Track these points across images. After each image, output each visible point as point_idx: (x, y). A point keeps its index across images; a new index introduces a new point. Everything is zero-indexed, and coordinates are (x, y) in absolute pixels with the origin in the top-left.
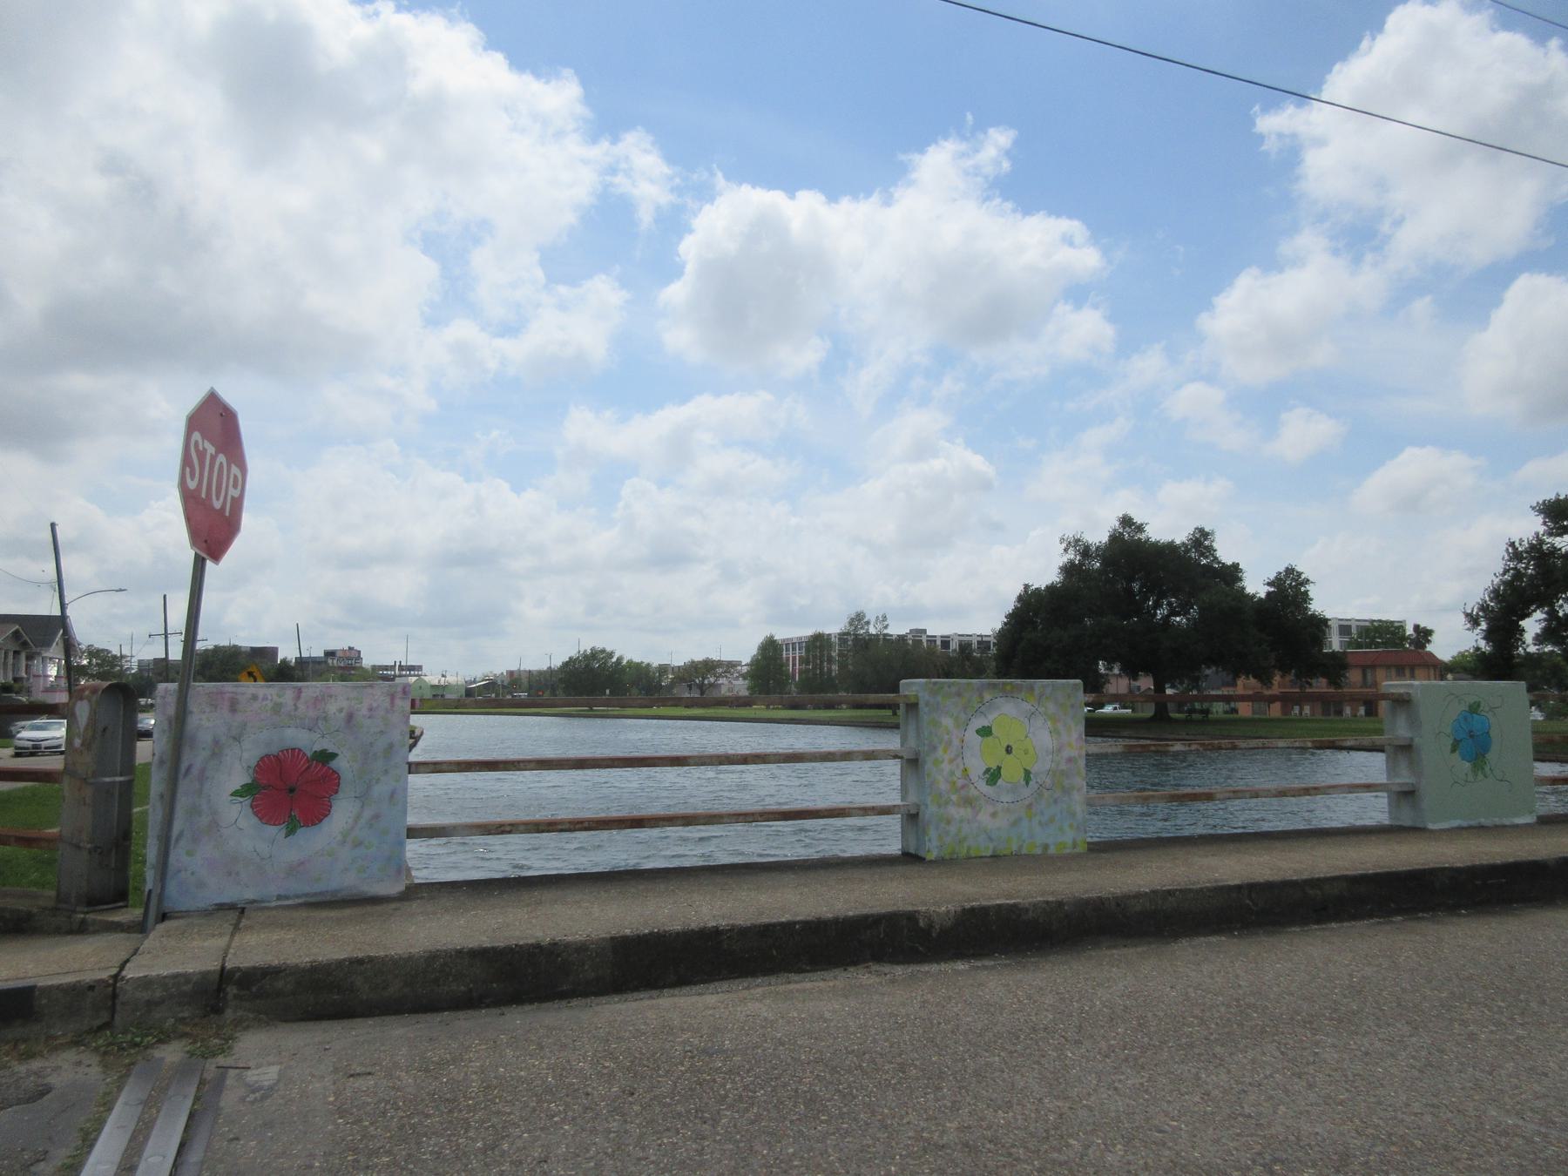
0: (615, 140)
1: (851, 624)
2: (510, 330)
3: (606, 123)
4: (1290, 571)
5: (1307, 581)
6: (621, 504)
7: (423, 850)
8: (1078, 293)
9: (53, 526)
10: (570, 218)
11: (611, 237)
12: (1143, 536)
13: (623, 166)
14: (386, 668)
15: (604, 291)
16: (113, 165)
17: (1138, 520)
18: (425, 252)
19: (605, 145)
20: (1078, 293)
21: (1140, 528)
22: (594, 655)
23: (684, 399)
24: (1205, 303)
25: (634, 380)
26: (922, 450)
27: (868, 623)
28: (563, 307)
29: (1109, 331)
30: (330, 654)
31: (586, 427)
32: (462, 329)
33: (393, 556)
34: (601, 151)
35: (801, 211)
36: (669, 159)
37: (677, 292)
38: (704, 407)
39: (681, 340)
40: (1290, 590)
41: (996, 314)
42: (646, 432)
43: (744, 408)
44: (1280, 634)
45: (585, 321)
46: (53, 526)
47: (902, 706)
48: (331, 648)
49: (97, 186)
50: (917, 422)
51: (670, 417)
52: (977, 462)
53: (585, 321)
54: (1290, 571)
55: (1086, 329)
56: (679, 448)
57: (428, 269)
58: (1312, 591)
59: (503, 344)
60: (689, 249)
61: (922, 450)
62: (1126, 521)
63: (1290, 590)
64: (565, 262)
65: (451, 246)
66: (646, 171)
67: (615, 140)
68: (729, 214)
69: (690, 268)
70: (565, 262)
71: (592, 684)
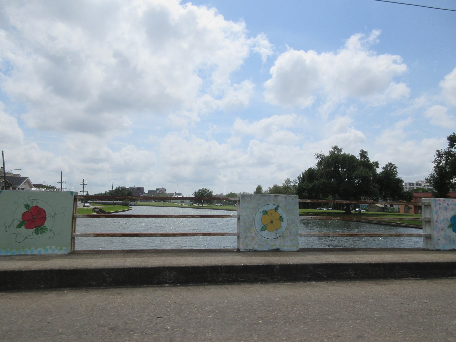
0: (255, 37)
1: (286, 182)
2: (219, 97)
3: (252, 32)
4: (390, 164)
5: (396, 167)
6: (249, 148)
7: (417, 240)
8: (397, 79)
9: (2, 151)
10: (241, 62)
11: (253, 68)
12: (342, 153)
13: (257, 44)
14: (172, 194)
15: (248, 85)
16: (117, 54)
17: (340, 148)
18: (199, 76)
19: (253, 39)
20: (397, 79)
21: (341, 150)
22: (204, 190)
23: (269, 116)
24: (442, 78)
25: (254, 112)
26: (342, 130)
27: (291, 182)
28: (235, 90)
29: (408, 90)
30: (158, 189)
31: (240, 125)
32: (207, 98)
33: (186, 162)
34: (249, 42)
35: (309, 57)
36: (271, 42)
37: (269, 83)
38: (275, 119)
39: (270, 98)
40: (390, 170)
41: (371, 86)
42: (257, 126)
43: (287, 119)
44: (387, 184)
45: (243, 93)
46: (2, 151)
47: (423, 206)
48: (158, 188)
49: (113, 61)
50: (341, 121)
51: (264, 122)
52: (360, 134)
53: (243, 93)
54: (390, 164)
55: (400, 90)
56: (267, 130)
57: (199, 81)
58: (398, 170)
59: (217, 101)
60: (273, 70)
61: (342, 130)
62: (336, 148)
63: (390, 170)
64: (238, 77)
65: (204, 73)
66: (264, 46)
67: (255, 37)
68: (287, 58)
69: (274, 76)
70: (238, 77)
71: (203, 198)
